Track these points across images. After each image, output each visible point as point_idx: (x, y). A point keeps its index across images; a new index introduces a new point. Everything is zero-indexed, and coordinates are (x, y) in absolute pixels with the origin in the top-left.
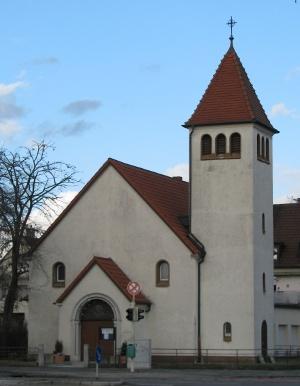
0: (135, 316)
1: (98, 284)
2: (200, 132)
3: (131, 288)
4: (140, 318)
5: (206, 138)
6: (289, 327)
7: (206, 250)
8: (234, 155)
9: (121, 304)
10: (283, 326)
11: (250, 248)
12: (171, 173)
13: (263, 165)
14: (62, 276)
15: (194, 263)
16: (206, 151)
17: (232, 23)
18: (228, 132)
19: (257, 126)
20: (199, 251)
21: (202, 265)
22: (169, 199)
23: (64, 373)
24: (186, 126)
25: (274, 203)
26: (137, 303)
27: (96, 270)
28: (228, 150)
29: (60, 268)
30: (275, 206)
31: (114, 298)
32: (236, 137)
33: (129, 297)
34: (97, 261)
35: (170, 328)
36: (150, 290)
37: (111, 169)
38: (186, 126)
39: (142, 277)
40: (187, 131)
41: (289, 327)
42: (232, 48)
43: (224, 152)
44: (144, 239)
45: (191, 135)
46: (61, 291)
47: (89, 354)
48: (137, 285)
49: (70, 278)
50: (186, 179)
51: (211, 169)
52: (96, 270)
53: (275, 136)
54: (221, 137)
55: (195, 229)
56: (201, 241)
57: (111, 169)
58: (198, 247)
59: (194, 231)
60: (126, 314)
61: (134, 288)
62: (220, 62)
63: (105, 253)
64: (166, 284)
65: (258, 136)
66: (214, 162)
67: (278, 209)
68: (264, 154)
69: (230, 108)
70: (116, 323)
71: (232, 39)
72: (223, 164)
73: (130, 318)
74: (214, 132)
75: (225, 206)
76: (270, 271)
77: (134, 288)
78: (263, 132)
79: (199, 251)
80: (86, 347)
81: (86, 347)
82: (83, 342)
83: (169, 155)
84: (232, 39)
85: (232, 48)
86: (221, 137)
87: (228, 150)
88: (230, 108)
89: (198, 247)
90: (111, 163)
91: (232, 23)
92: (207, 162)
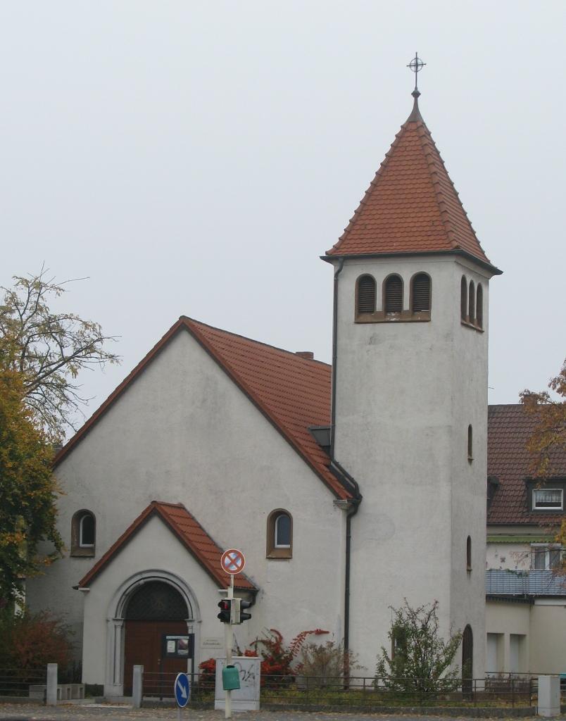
0: (235, 614)
1: (157, 553)
2: (353, 274)
3: (227, 561)
4: (245, 617)
5: (366, 283)
6: (507, 638)
7: (364, 491)
8: (418, 316)
9: (203, 597)
10: (495, 637)
11: (445, 490)
12: (292, 344)
13: (471, 334)
14: (90, 535)
15: (339, 517)
16: (364, 306)
17: (416, 65)
18: (406, 272)
19: (462, 261)
20: (348, 495)
21: (354, 521)
22: (293, 400)
23: (462, 224)
24: (329, 258)
25: (491, 403)
26: (237, 590)
27: (155, 528)
28: (406, 305)
29: (86, 522)
30: (491, 407)
31: (192, 585)
32: (422, 282)
33: (219, 580)
34: (155, 511)
35: (296, 605)
36: (257, 566)
37: (185, 340)
38: (329, 258)
39: (241, 537)
40: (330, 268)
41: (507, 638)
42: (416, 114)
43: (398, 308)
44: (239, 472)
45: (337, 275)
46: (87, 566)
47: (144, 683)
48: (239, 556)
49: (105, 538)
50: (324, 355)
51: (373, 340)
52: (155, 528)
53: (494, 279)
54: (394, 282)
55: (342, 454)
56: (354, 476)
57: (185, 340)
58: (347, 487)
59: (340, 455)
60: (219, 610)
61: (233, 562)
62: (383, 158)
63: (172, 494)
64: (286, 556)
65: (464, 280)
66: (381, 329)
67: (494, 411)
68: (473, 316)
69: (409, 239)
70: (193, 628)
71: (416, 94)
72: (396, 333)
73: (224, 617)
74: (380, 273)
75: (404, 413)
76: (479, 530)
77: (233, 562)
78: (471, 271)
79: (348, 495)
80: (138, 670)
81: (138, 670)
82: (130, 660)
83: (296, 312)
84: (416, 94)
85: (416, 114)
86: (394, 282)
87: (406, 305)
88: (409, 239)
89: (347, 487)
90: (185, 326)
91: (416, 65)
92: (368, 326)
